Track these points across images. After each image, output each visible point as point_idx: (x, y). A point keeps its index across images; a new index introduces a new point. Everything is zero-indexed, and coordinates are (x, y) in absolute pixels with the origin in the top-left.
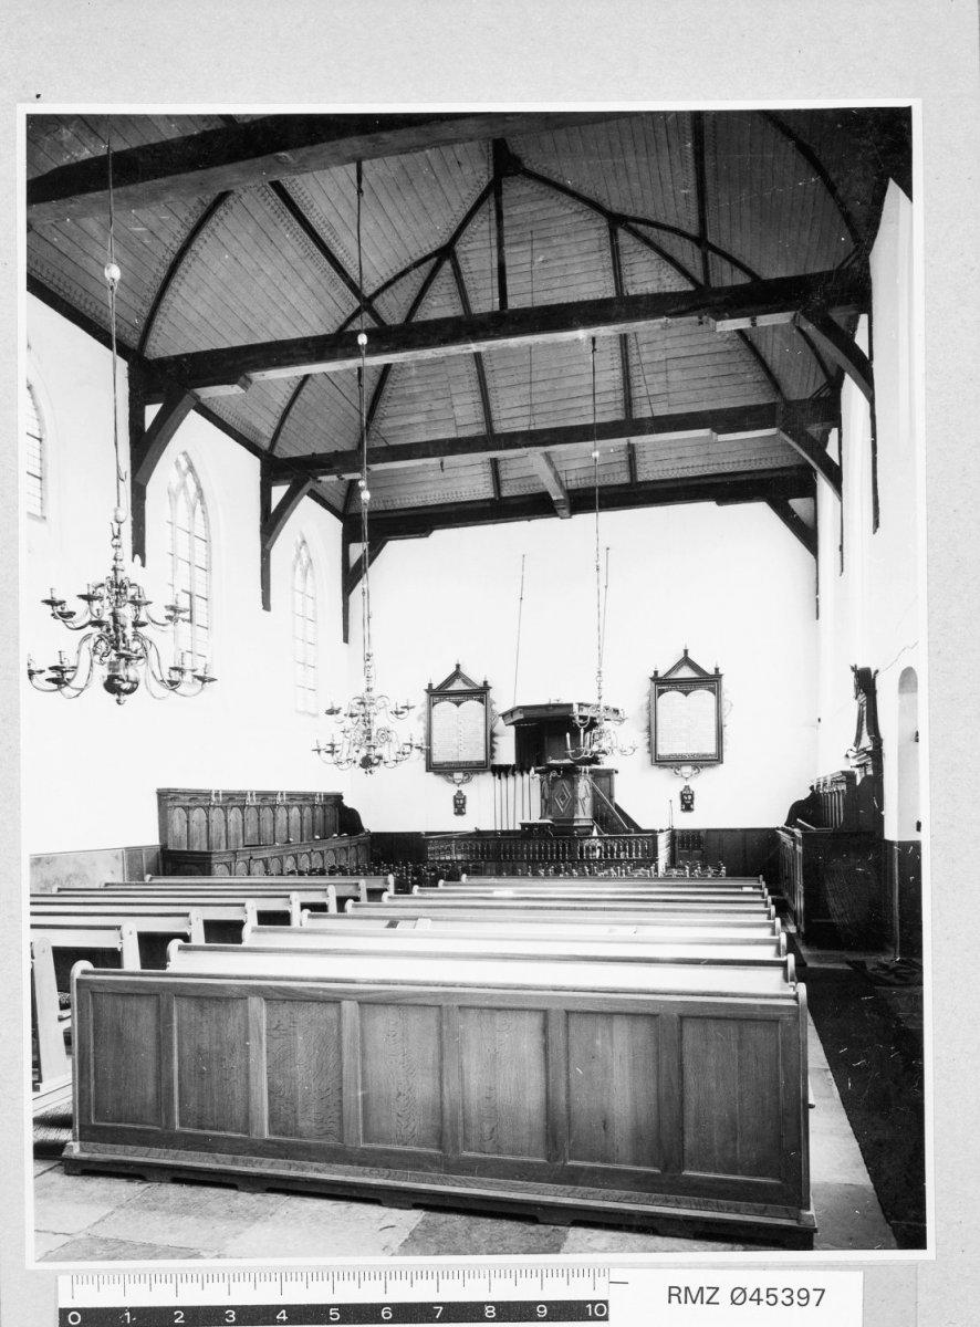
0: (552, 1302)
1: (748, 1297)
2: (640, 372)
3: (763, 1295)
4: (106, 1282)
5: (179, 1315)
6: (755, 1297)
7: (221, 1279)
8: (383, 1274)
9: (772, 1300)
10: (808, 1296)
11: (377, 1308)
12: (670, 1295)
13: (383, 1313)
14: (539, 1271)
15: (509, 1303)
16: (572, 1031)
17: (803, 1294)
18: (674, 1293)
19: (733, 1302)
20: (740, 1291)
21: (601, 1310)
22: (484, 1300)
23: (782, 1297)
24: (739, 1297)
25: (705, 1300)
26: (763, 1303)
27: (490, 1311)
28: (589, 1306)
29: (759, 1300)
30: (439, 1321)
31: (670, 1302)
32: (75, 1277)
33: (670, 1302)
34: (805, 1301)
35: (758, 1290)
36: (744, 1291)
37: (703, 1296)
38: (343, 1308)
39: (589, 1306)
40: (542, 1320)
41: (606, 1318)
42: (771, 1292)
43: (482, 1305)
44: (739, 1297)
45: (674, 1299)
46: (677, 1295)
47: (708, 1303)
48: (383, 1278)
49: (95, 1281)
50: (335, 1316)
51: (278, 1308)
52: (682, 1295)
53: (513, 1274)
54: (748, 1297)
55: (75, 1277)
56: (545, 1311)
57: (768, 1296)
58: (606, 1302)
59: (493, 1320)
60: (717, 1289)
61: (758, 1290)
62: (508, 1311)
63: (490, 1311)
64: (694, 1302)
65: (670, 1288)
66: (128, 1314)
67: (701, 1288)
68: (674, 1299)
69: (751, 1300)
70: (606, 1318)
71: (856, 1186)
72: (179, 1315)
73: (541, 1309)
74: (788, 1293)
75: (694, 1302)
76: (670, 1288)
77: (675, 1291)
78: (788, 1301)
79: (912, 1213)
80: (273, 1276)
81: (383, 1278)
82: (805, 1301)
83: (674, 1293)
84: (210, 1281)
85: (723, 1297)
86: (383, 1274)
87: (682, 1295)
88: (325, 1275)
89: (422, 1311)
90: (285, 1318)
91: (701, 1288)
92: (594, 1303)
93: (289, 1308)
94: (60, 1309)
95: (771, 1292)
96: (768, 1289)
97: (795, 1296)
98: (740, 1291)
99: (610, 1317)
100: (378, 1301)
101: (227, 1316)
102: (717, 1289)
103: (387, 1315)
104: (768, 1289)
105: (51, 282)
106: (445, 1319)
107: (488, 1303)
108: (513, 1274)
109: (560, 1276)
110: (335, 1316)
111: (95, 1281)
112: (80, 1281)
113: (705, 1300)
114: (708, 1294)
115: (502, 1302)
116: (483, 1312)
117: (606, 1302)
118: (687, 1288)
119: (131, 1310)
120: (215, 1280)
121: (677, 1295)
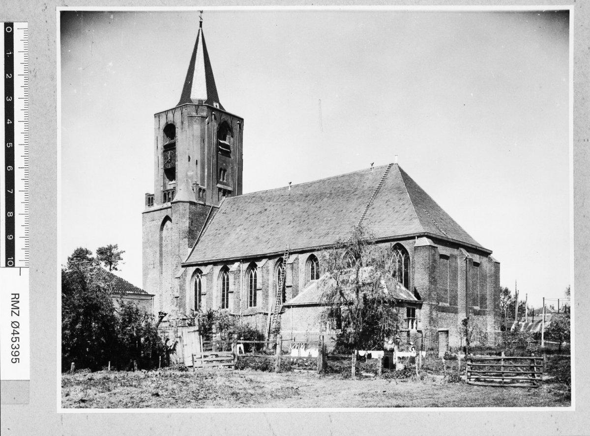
1: (15, 329)
3: (16, 336)
4: (25, 44)
5: (10, 76)
6: (15, 332)
7: (26, 164)
8: (28, 167)
9: (14, 340)
11: (13, 164)
12: (15, 294)
13: (10, 167)
14: (28, 236)
17: (17, 354)
18: (16, 298)
19: (13, 323)
20: (13, 324)
21: (10, 263)
22: (15, 235)
23: (15, 344)
24: (15, 325)
25: (13, 310)
27: (10, 214)
28: (12, 258)
29: (14, 334)
31: (12, 294)
33: (12, 294)
35: (18, 333)
36: (18, 327)
37: (15, 308)
39: (12, 258)
41: (7, 266)
42: (17, 339)
43: (6, 125)
44: (15, 325)
45: (14, 296)
46: (15, 297)
47: (12, 311)
49: (25, 39)
50: (9, 145)
51: (13, 120)
52: (15, 300)
56: (10, 239)
57: (15, 338)
60: (18, 315)
61: (18, 333)
63: (10, 214)
64: (12, 305)
65: (18, 294)
66: (11, 53)
67: (18, 308)
68: (14, 296)
69: (14, 330)
72: (10, 76)
73: (11, 237)
74: (17, 347)
75: (12, 305)
76: (18, 294)
77: (17, 296)
78: (14, 347)
80: (27, 118)
83: (16, 298)
84: (26, 241)
85: (15, 318)
86: (28, 167)
87: (15, 300)
90: (8, 123)
91: (18, 308)
92: (14, 260)
94: (13, 23)
95: (17, 339)
96: (19, 338)
97: (16, 350)
101: (9, 98)
102: (18, 315)
103: (9, 168)
104: (19, 338)
105: (381, 195)
107: (14, 213)
109: (26, 222)
110: (9, 145)
111: (25, 39)
112: (25, 32)
113: (13, 310)
114: (16, 311)
116: (10, 211)
118: (18, 302)
119: (12, 55)
120: (26, 162)
121: (15, 297)
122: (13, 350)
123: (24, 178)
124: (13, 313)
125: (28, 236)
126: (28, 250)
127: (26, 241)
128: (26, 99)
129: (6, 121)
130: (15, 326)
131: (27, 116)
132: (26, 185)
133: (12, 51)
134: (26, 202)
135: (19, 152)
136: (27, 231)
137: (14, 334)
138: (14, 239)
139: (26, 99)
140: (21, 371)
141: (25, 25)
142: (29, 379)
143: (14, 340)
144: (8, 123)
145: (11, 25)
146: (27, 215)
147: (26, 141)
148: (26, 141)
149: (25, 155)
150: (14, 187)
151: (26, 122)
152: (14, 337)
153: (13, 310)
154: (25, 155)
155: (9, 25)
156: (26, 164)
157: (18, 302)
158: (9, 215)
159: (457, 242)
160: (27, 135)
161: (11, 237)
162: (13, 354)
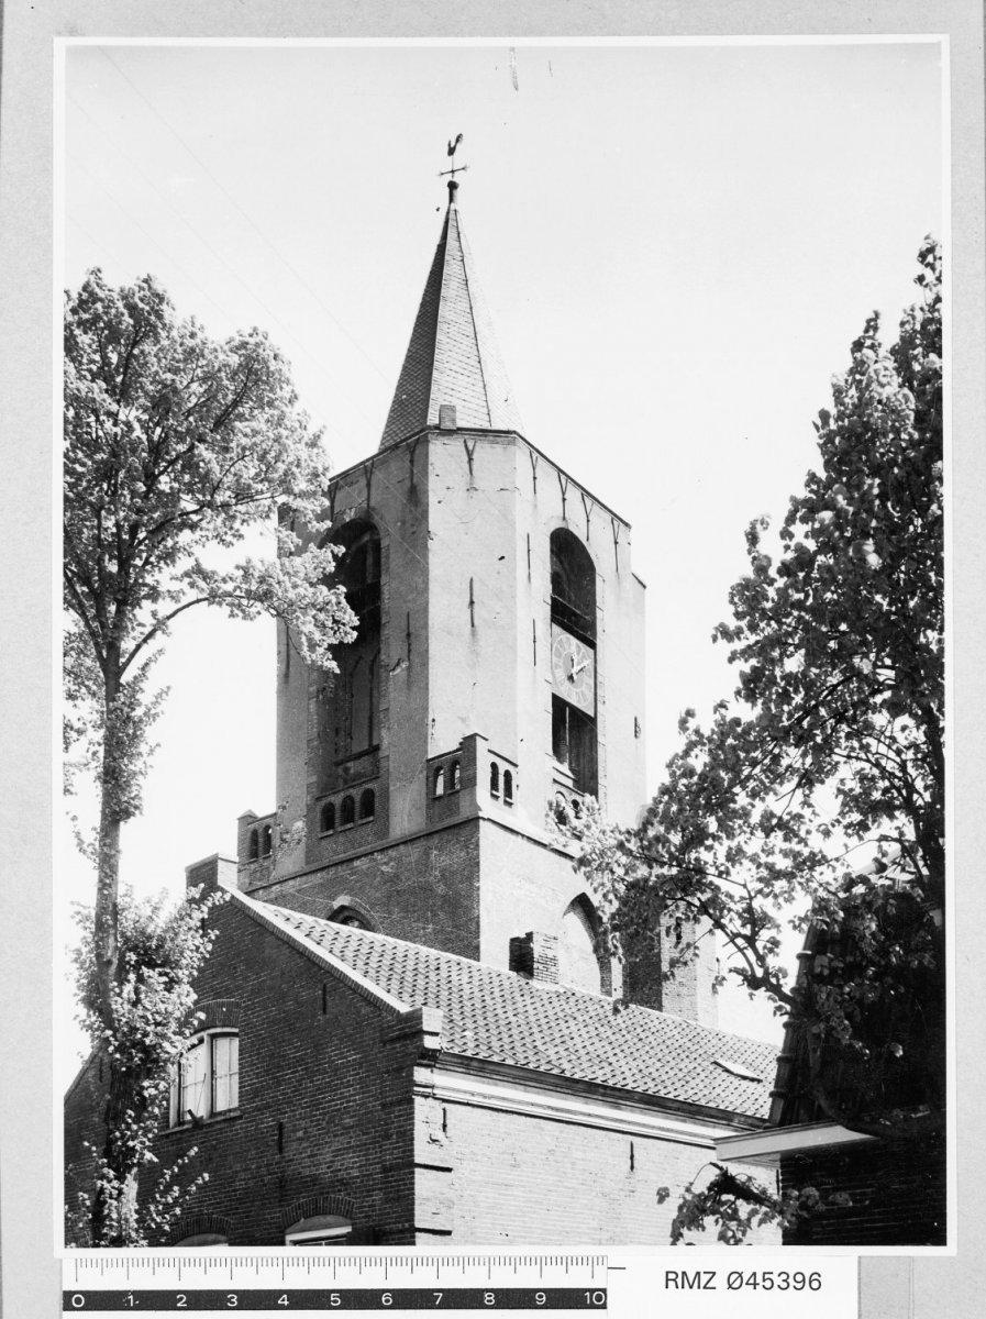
1: (745, 1282)
6: (752, 1281)
9: (768, 1284)
12: (667, 1280)
13: (383, 1299)
15: (507, 1289)
17: (799, 1278)
19: (730, 1286)
21: (599, 1298)
23: (778, 1281)
25: (702, 1285)
28: (588, 1294)
29: (755, 1284)
34: (801, 1285)
35: (754, 1274)
36: (740, 1275)
39: (588, 1294)
41: (604, 1307)
42: (767, 1276)
45: (671, 1284)
47: (705, 1287)
50: (335, 1302)
51: (280, 1293)
52: (679, 1280)
56: (544, 1298)
58: (604, 1291)
60: (714, 1273)
61: (754, 1274)
63: (489, 1298)
64: (691, 1287)
66: (131, 1297)
67: (698, 1273)
68: (671, 1284)
70: (604, 1307)
73: (541, 1297)
74: (784, 1277)
75: (691, 1287)
77: (672, 1276)
78: (784, 1285)
82: (801, 1285)
85: (720, 1281)
87: (679, 1280)
90: (286, 1303)
91: (698, 1273)
92: (592, 1291)
94: (65, 1292)
95: (767, 1276)
96: (764, 1273)
97: (791, 1280)
101: (229, 1300)
102: (714, 1273)
103: (387, 1301)
104: (764, 1273)
106: (445, 1305)
110: (335, 1302)
113: (702, 1285)
117: (604, 1291)
119: (134, 1293)
122: (791, 1287)
129: (282, 1307)
130: (739, 1281)
144: (286, 1303)
145: (68, 1295)
147: (327, 1263)
149: (358, 1264)
152: (762, 1284)
153: (702, 1285)
154: (358, 1264)
155: (69, 1301)
157: (684, 1273)
158: (491, 1301)
162: (799, 1286)
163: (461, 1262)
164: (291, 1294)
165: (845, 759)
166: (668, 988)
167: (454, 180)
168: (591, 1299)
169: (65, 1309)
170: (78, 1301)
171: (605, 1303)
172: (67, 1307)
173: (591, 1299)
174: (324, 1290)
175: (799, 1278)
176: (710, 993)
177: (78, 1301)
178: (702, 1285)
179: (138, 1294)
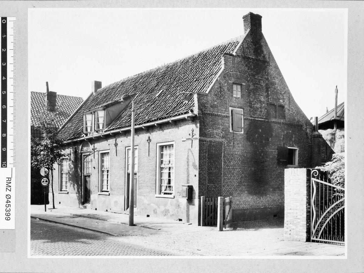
0: (7, 152)
1: (8, 199)
2: (209, 132)
6: (8, 201)
7: (14, 140)
8: (15, 106)
9: (7, 206)
10: (8, 220)
12: (9, 178)
13: (4, 106)
14: (15, 149)
15: (7, 140)
16: (70, 152)
17: (9, 214)
19: (7, 195)
20: (10, 197)
21: (4, 165)
22: (7, 134)
23: (8, 209)
24: (8, 197)
25: (7, 188)
26: (6, 203)
28: (5, 162)
29: (7, 202)
30: (2, 121)
32: (15, 22)
34: (7, 215)
35: (10, 202)
36: (10, 198)
38: (6, 95)
39: (5, 162)
40: (2, 149)
41: (2, 167)
42: (9, 206)
43: (6, 133)
45: (8, 179)
47: (7, 188)
48: (14, 106)
50: (4, 93)
51: (6, 77)
52: (9, 181)
53: (15, 120)
54: (8, 199)
55: (15, 22)
56: (4, 150)
58: (6, 167)
59: (2, 136)
60: (10, 191)
61: (10, 202)
62: (4, 140)
63: (4, 135)
64: (7, 185)
66: (5, 36)
67: (10, 187)
68: (8, 179)
70: (2, 167)
71: (87, 203)
73: (5, 149)
74: (9, 210)
75: (7, 185)
77: (10, 179)
78: (7, 210)
79: (208, 223)
81: (14, 106)
82: (7, 215)
84: (14, 152)
85: (8, 192)
86: (15, 106)
87: (9, 181)
88: (15, 90)
89: (4, 59)
90: (3, 79)
91: (10, 187)
92: (6, 164)
93: (6, 80)
94: (6, 18)
95: (9, 206)
96: (10, 205)
97: (8, 212)
98: (10, 197)
99: (2, 168)
100: (7, 105)
101: (4, 63)
102: (10, 191)
103: (4, 107)
104: (10, 205)
106: (2, 123)
108: (15, 120)
110: (4, 93)
113: (7, 188)
114: (9, 188)
115: (7, 139)
117: (6, 167)
119: (6, 37)
122: (6, 212)
123: (13, 113)
124: (7, 189)
125: (15, 149)
126: (15, 107)
127: (14, 152)
128: (14, 64)
129: (2, 78)
130: (8, 198)
131: (15, 47)
132: (14, 153)
133: (6, 35)
134: (14, 57)
135: (10, 68)
136: (15, 146)
137: (7, 202)
138: (6, 150)
139: (14, 64)
140: (11, 225)
141: (14, 19)
142: (14, 229)
143: (7, 206)
144: (3, 79)
145: (6, 18)
146: (15, 136)
147: (14, 90)
148: (14, 90)
149: (14, 99)
150: (7, 118)
151: (14, 79)
152: (7, 204)
153: (7, 188)
154: (14, 99)
155: (4, 19)
156: (14, 140)
157: (10, 183)
158: (4, 135)
159: (293, 161)
160: (14, 86)
161: (5, 149)
162: (7, 214)
163: (14, 127)
164: (6, 80)
165: (195, 252)
166: (336, 149)
167: (190, 184)
168: (4, 163)
169: (2, 18)
170: (4, 21)
171: (3, 167)
172: (2, 18)
173: (4, 163)
174: (7, 89)
175: (9, 219)
176: (175, 196)
177: (4, 21)
178: (7, 188)
179: (6, 38)
